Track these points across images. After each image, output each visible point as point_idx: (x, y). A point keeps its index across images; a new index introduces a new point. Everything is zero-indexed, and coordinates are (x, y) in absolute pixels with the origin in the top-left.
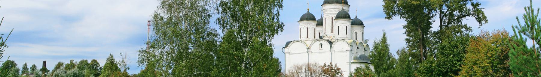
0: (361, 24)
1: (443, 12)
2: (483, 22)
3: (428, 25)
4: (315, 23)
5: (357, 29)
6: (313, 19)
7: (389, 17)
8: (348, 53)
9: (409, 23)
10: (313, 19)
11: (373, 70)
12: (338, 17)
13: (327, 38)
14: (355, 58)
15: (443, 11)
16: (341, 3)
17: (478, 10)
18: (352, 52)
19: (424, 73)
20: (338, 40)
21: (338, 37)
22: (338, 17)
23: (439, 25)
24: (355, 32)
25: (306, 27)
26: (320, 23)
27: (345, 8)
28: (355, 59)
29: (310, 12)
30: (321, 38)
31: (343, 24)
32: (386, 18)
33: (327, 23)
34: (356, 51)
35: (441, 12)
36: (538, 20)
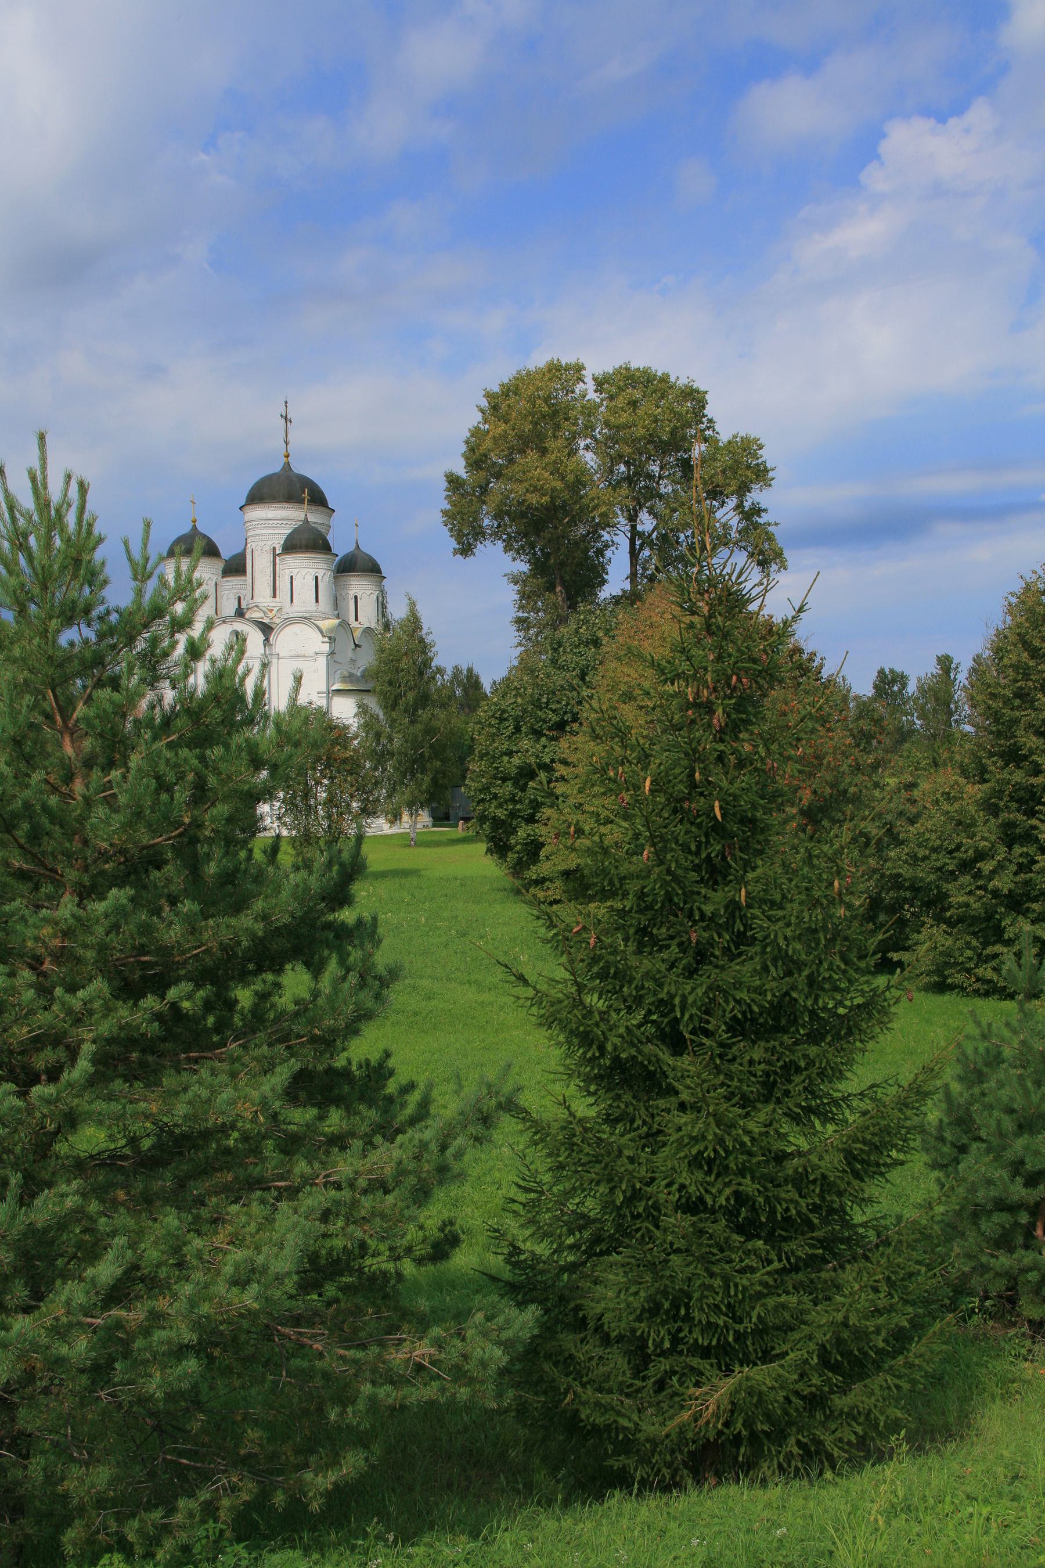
0: (372, 569)
1: (641, 534)
2: (774, 567)
3: (596, 576)
4: (220, 565)
5: (360, 587)
6: (211, 551)
7: (466, 550)
8: (322, 661)
9: (539, 567)
10: (211, 551)
11: (381, 716)
12: (291, 546)
13: (257, 615)
14: (350, 678)
15: (639, 528)
16: (302, 502)
17: (756, 526)
18: (337, 657)
19: (490, 726)
20: (289, 621)
21: (290, 611)
22: (291, 546)
23: (628, 571)
24: (352, 593)
25: (313, 572)
26: (236, 567)
27: (315, 518)
28: (350, 678)
29: (201, 528)
30: (240, 613)
31: (306, 571)
32: (455, 552)
33: (260, 564)
34: (350, 654)
35: (634, 534)
36: (197, 594)
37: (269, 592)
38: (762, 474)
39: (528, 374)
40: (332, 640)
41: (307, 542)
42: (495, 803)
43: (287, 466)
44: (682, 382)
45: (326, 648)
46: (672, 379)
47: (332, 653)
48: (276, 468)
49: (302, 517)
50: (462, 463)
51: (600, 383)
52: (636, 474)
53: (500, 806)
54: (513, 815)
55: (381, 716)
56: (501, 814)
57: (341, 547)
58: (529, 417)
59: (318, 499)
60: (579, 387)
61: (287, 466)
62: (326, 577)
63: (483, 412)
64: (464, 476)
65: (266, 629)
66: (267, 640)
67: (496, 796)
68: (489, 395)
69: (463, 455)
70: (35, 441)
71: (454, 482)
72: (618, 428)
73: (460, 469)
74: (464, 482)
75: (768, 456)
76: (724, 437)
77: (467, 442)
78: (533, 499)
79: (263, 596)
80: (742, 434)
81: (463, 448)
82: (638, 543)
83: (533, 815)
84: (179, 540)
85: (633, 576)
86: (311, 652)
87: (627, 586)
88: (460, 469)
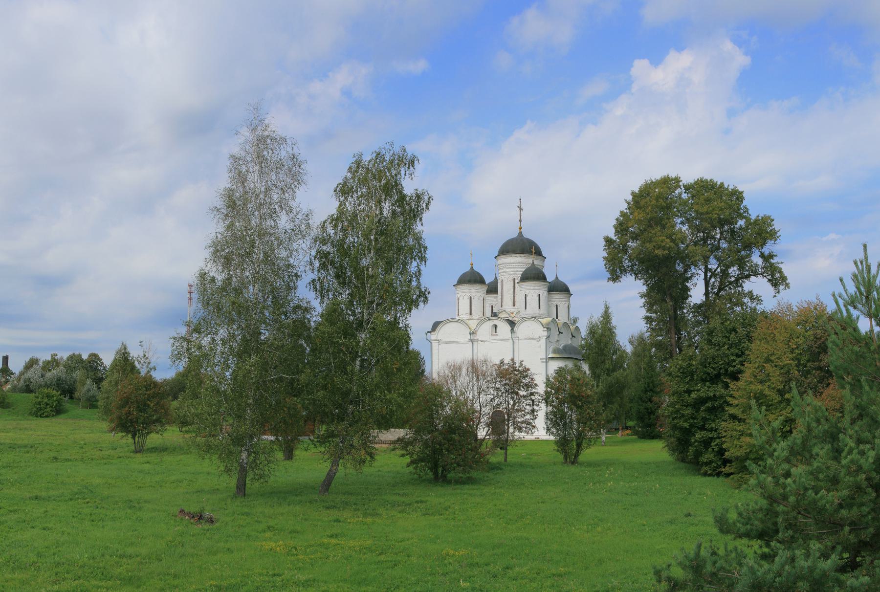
2: (781, 287)
4: (485, 288)
5: (559, 299)
11: (588, 372)
12: (525, 278)
13: (505, 316)
15: (709, 266)
17: (772, 265)
18: (551, 339)
20: (524, 319)
21: (525, 313)
22: (525, 278)
24: (555, 303)
25: (538, 292)
26: (493, 289)
27: (537, 262)
28: (554, 352)
31: (534, 290)
32: (609, 279)
33: (506, 288)
34: (556, 337)
35: (707, 270)
37: (511, 303)
38: (773, 235)
39: (652, 182)
40: (549, 329)
41: (533, 275)
42: (682, 419)
43: (520, 233)
44: (731, 187)
45: (545, 334)
46: (726, 186)
47: (548, 337)
48: (514, 235)
49: (531, 261)
50: (613, 230)
51: (688, 188)
52: (708, 237)
53: (686, 421)
54: (691, 426)
55: (588, 372)
56: (686, 425)
57: (550, 278)
58: (653, 205)
59: (538, 253)
60: (678, 191)
61: (520, 233)
62: (544, 293)
63: (628, 203)
64: (614, 238)
65: (512, 323)
66: (512, 330)
67: (683, 416)
68: (633, 193)
69: (614, 226)
70: (862, 248)
71: (609, 241)
72: (702, 214)
73: (612, 234)
74: (615, 241)
75: (776, 225)
76: (753, 217)
77: (617, 219)
78: (659, 252)
79: (508, 306)
80: (761, 215)
81: (615, 222)
82: (709, 274)
83: (704, 425)
84: (420, 274)
85: (707, 294)
86: (537, 336)
87: (704, 299)
88: (612, 234)
